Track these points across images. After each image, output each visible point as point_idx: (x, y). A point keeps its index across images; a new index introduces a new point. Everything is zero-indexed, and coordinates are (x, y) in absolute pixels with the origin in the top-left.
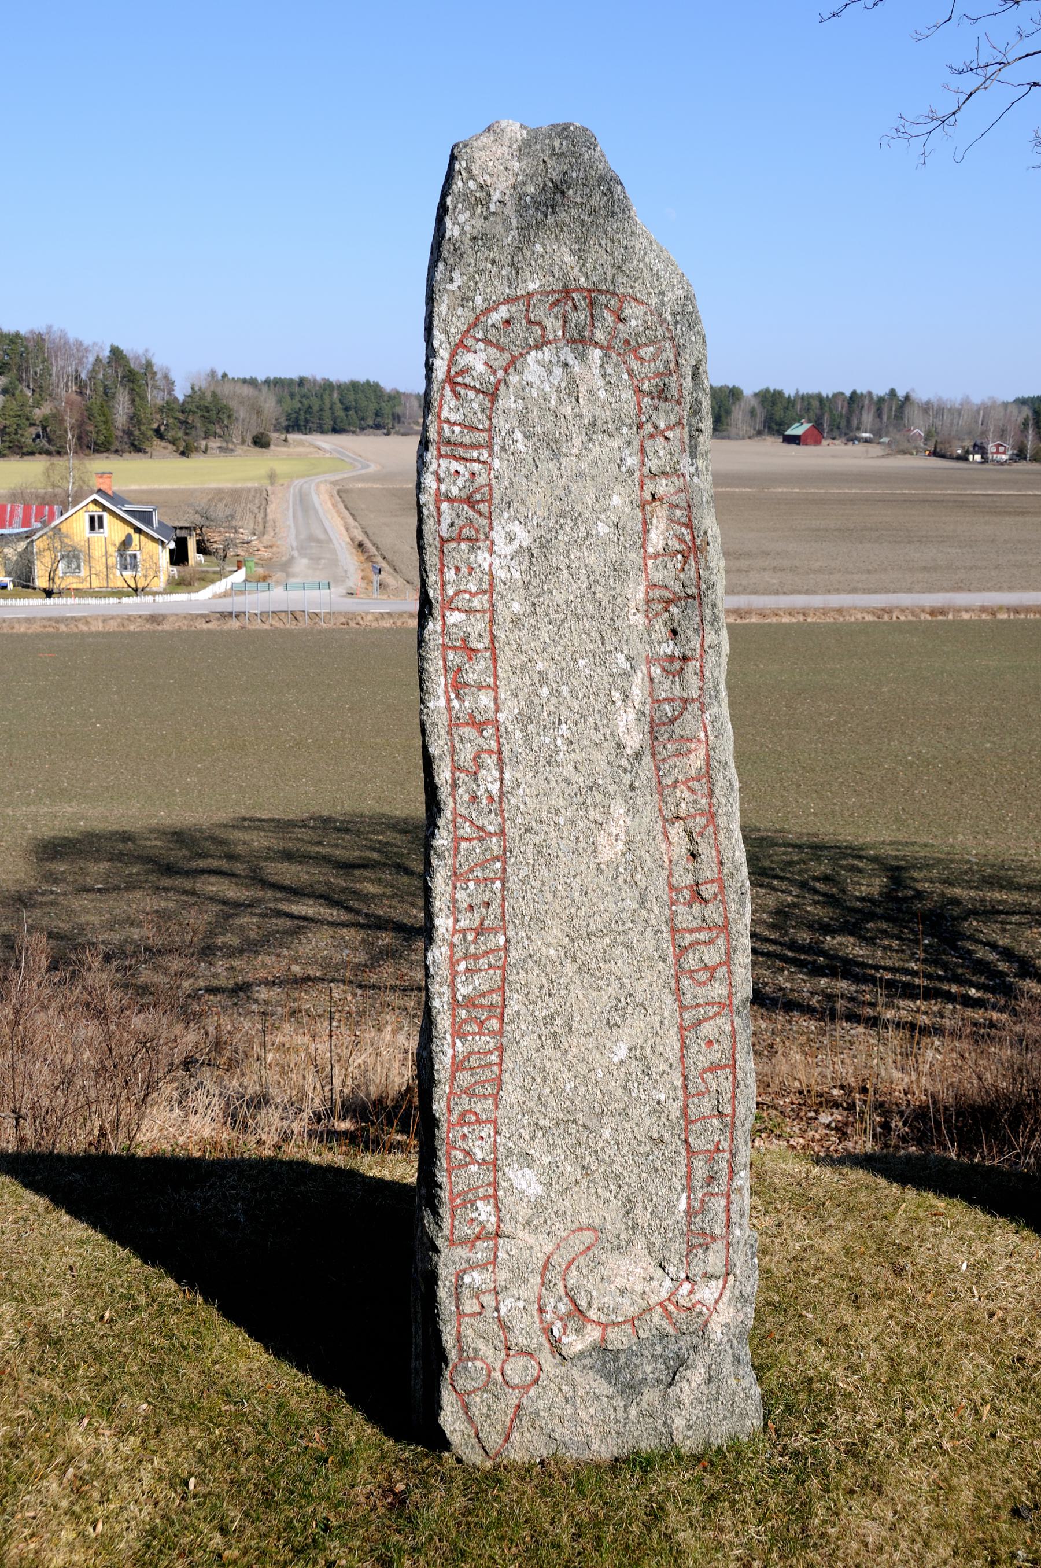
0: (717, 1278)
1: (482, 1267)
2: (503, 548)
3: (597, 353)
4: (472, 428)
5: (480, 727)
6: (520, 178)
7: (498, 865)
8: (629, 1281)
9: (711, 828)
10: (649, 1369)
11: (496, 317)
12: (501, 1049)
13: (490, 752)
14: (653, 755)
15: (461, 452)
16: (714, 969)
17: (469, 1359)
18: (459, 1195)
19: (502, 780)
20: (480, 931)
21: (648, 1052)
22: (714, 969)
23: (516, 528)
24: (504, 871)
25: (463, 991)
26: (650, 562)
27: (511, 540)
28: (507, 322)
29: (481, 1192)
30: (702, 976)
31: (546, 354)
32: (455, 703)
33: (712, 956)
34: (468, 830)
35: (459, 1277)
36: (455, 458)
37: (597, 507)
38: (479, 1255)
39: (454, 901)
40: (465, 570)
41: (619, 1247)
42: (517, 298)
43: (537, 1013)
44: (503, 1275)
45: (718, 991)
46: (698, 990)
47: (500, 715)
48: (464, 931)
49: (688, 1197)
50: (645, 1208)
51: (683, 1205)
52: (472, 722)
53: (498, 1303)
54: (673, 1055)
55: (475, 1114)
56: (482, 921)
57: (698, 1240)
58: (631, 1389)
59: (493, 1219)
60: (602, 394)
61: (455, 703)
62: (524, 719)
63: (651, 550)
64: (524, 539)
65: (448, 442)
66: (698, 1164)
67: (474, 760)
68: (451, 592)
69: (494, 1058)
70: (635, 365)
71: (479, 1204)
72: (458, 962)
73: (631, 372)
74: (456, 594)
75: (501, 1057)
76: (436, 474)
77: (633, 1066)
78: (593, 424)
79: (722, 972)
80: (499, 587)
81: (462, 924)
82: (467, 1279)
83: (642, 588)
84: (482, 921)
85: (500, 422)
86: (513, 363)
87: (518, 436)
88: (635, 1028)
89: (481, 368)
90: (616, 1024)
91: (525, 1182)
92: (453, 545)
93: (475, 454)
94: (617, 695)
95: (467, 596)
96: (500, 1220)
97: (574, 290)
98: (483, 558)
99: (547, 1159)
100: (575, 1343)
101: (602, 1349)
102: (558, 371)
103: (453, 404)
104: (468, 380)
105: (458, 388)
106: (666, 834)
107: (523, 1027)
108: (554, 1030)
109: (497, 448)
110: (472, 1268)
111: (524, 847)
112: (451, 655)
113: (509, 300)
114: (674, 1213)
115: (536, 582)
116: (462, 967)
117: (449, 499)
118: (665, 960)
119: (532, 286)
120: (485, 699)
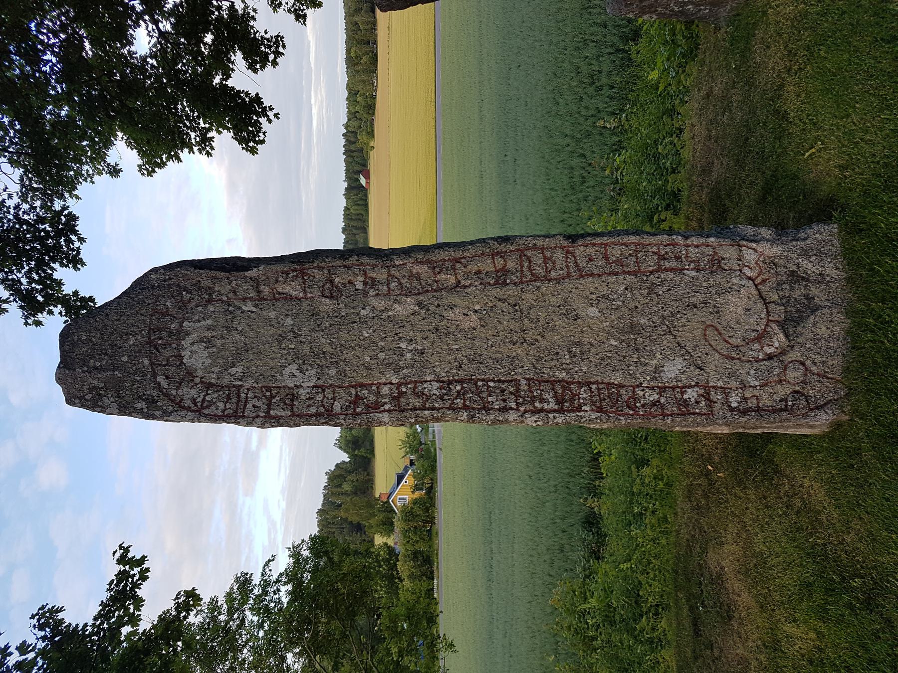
0: (741, 251)
1: (727, 395)
2: (299, 379)
3: (185, 324)
4: (228, 397)
5: (401, 394)
6: (86, 369)
7: (480, 383)
8: (739, 308)
9: (462, 261)
10: (798, 293)
11: (164, 383)
12: (589, 384)
13: (416, 387)
14: (419, 294)
15: (241, 404)
16: (545, 258)
17: (786, 405)
18: (680, 410)
19: (430, 381)
20: (517, 394)
21: (594, 296)
22: (545, 258)
23: (287, 371)
24: (483, 380)
25: (552, 405)
26: (309, 295)
27: (294, 375)
28: (167, 377)
29: (678, 396)
30: (549, 266)
31: (186, 354)
32: (387, 407)
33: (538, 260)
34: (459, 401)
35: (732, 410)
36: (245, 405)
37: (276, 326)
38: (720, 397)
39: (499, 410)
40: (310, 402)
41: (718, 312)
42: (153, 370)
43: (568, 362)
44: (733, 384)
45: (559, 256)
46: (558, 267)
47: (394, 381)
48: (517, 404)
49: (687, 270)
50: (693, 297)
51: (694, 273)
52: (397, 398)
53: (750, 386)
54: (598, 280)
55: (629, 399)
56: (511, 393)
57: (716, 265)
58: (810, 307)
59: (696, 389)
60: (210, 322)
61: (387, 407)
62: (397, 370)
63: (301, 295)
64: (293, 368)
65: (236, 412)
66: (667, 265)
67: (419, 397)
68: (322, 410)
69: (594, 387)
70: (193, 304)
71: (685, 397)
72: (535, 407)
73: (197, 306)
74: (323, 406)
75: (593, 383)
76: (763, 40)
77: (603, 306)
78: (227, 328)
79: (548, 254)
80: (321, 382)
81: (513, 405)
82: (734, 405)
83: (323, 299)
84: (511, 393)
85: (225, 382)
86: (190, 373)
87: (233, 370)
88: (578, 303)
89: (193, 392)
90: (576, 315)
91: (673, 370)
92: (295, 408)
93: (243, 395)
94: (384, 315)
95: (325, 400)
96: (697, 384)
97: (149, 338)
98: (303, 393)
99: (659, 356)
100: (779, 340)
101: (782, 325)
102: (195, 348)
103: (213, 408)
104: (199, 399)
105: (205, 405)
106: (465, 287)
107: (576, 369)
108: (578, 350)
109: (240, 383)
110: (728, 401)
111: (469, 369)
112: (359, 410)
113: (155, 375)
114: (697, 279)
115: (318, 361)
116: (538, 405)
117: (268, 412)
118: (539, 287)
119: (146, 362)
120: (385, 390)
